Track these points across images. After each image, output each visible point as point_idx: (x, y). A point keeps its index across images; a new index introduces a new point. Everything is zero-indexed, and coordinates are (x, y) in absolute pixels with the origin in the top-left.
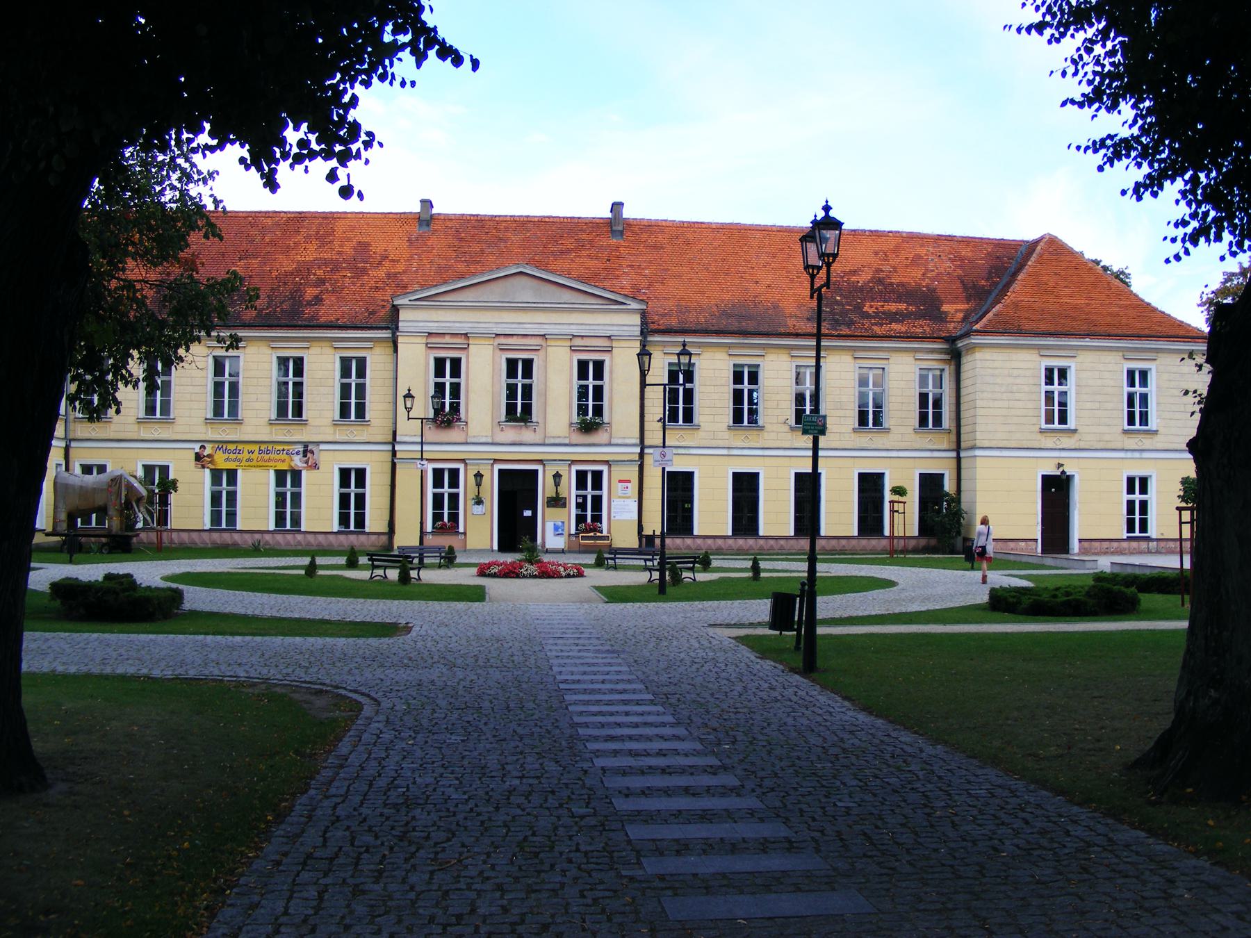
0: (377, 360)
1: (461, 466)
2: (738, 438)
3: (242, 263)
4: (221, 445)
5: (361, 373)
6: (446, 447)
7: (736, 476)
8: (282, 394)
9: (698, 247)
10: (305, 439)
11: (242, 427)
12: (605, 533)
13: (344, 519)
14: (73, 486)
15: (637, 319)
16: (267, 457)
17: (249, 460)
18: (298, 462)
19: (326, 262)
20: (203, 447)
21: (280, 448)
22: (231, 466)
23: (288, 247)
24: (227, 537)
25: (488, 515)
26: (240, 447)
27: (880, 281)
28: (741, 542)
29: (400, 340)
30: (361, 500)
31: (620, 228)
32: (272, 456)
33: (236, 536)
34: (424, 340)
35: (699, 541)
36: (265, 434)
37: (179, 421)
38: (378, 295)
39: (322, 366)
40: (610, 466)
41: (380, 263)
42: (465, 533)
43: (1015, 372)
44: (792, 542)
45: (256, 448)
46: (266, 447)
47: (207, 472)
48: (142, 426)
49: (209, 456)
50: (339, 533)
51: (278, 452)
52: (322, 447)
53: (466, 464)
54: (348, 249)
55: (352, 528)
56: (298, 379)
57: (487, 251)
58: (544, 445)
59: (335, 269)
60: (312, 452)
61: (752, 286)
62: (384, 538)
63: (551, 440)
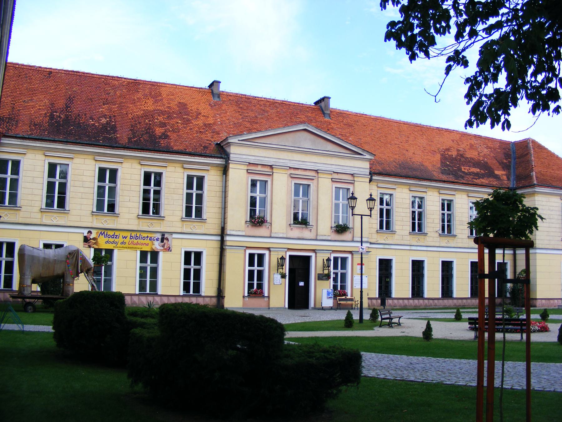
0: (212, 180)
1: (267, 252)
2: (414, 240)
3: (106, 106)
4: (103, 231)
5: (200, 186)
6: (258, 240)
7: (443, 262)
8: (146, 199)
9: (370, 128)
10: (163, 230)
11: (119, 219)
12: (349, 297)
13: (186, 287)
14: (38, 258)
15: (367, 165)
16: (135, 241)
17: (123, 243)
18: (157, 246)
19: (162, 113)
20: (90, 232)
21: (146, 235)
22: (110, 246)
23: (134, 100)
24: (194, 300)
25: (283, 284)
26: (117, 233)
27: (462, 156)
28: (416, 301)
29: (231, 166)
30: (198, 273)
31: (329, 112)
32: (140, 241)
33: (157, 299)
34: (246, 168)
35: (426, 301)
36: (134, 224)
37: (72, 212)
38: (203, 136)
39: (174, 179)
40: (352, 254)
41: (197, 117)
42: (269, 297)
43: (551, 208)
44: (469, 301)
45: (128, 234)
46: (136, 234)
47: (92, 250)
48: (44, 214)
49: (94, 239)
50: (184, 296)
51: (144, 238)
52: (174, 236)
53: (270, 251)
54: (173, 105)
55: (191, 293)
56: (157, 188)
57: (259, 116)
58: (316, 240)
59: (170, 117)
60: (167, 239)
61: (405, 152)
62: (214, 300)
63: (318, 242)
